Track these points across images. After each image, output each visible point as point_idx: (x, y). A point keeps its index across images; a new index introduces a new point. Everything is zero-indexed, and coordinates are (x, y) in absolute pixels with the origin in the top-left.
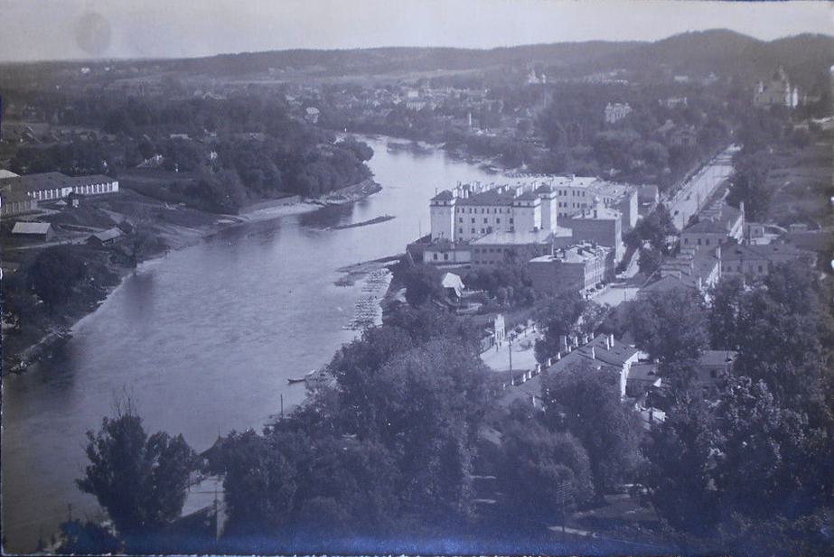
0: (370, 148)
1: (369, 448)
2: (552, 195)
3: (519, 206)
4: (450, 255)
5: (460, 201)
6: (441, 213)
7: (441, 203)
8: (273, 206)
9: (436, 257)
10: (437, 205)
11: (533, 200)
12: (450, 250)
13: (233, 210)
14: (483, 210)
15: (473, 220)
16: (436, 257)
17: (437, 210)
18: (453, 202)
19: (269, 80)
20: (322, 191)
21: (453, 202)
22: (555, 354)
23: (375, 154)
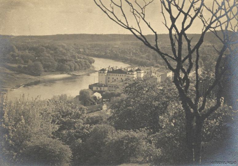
0: (93, 60)
1: (166, 114)
2: (142, 72)
3: (129, 74)
4: (102, 88)
5: (109, 72)
6: (102, 75)
7: (102, 72)
8: (53, 74)
9: (97, 89)
10: (101, 72)
11: (133, 72)
12: (102, 86)
13: (38, 75)
14: (112, 75)
15: (109, 78)
16: (97, 89)
17: (101, 74)
18: (106, 72)
19: (64, 43)
20: (71, 70)
21: (106, 72)
22: (215, 74)
23: (95, 61)
